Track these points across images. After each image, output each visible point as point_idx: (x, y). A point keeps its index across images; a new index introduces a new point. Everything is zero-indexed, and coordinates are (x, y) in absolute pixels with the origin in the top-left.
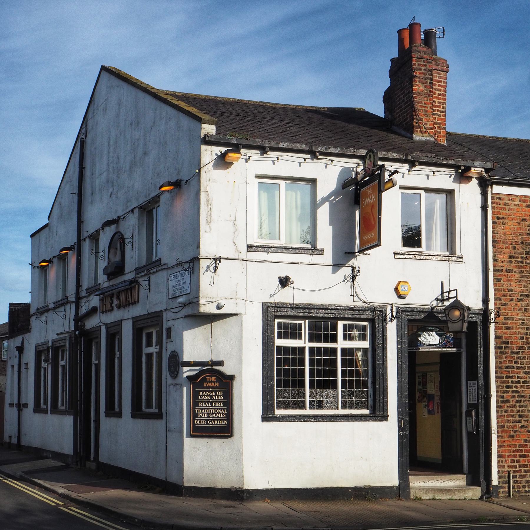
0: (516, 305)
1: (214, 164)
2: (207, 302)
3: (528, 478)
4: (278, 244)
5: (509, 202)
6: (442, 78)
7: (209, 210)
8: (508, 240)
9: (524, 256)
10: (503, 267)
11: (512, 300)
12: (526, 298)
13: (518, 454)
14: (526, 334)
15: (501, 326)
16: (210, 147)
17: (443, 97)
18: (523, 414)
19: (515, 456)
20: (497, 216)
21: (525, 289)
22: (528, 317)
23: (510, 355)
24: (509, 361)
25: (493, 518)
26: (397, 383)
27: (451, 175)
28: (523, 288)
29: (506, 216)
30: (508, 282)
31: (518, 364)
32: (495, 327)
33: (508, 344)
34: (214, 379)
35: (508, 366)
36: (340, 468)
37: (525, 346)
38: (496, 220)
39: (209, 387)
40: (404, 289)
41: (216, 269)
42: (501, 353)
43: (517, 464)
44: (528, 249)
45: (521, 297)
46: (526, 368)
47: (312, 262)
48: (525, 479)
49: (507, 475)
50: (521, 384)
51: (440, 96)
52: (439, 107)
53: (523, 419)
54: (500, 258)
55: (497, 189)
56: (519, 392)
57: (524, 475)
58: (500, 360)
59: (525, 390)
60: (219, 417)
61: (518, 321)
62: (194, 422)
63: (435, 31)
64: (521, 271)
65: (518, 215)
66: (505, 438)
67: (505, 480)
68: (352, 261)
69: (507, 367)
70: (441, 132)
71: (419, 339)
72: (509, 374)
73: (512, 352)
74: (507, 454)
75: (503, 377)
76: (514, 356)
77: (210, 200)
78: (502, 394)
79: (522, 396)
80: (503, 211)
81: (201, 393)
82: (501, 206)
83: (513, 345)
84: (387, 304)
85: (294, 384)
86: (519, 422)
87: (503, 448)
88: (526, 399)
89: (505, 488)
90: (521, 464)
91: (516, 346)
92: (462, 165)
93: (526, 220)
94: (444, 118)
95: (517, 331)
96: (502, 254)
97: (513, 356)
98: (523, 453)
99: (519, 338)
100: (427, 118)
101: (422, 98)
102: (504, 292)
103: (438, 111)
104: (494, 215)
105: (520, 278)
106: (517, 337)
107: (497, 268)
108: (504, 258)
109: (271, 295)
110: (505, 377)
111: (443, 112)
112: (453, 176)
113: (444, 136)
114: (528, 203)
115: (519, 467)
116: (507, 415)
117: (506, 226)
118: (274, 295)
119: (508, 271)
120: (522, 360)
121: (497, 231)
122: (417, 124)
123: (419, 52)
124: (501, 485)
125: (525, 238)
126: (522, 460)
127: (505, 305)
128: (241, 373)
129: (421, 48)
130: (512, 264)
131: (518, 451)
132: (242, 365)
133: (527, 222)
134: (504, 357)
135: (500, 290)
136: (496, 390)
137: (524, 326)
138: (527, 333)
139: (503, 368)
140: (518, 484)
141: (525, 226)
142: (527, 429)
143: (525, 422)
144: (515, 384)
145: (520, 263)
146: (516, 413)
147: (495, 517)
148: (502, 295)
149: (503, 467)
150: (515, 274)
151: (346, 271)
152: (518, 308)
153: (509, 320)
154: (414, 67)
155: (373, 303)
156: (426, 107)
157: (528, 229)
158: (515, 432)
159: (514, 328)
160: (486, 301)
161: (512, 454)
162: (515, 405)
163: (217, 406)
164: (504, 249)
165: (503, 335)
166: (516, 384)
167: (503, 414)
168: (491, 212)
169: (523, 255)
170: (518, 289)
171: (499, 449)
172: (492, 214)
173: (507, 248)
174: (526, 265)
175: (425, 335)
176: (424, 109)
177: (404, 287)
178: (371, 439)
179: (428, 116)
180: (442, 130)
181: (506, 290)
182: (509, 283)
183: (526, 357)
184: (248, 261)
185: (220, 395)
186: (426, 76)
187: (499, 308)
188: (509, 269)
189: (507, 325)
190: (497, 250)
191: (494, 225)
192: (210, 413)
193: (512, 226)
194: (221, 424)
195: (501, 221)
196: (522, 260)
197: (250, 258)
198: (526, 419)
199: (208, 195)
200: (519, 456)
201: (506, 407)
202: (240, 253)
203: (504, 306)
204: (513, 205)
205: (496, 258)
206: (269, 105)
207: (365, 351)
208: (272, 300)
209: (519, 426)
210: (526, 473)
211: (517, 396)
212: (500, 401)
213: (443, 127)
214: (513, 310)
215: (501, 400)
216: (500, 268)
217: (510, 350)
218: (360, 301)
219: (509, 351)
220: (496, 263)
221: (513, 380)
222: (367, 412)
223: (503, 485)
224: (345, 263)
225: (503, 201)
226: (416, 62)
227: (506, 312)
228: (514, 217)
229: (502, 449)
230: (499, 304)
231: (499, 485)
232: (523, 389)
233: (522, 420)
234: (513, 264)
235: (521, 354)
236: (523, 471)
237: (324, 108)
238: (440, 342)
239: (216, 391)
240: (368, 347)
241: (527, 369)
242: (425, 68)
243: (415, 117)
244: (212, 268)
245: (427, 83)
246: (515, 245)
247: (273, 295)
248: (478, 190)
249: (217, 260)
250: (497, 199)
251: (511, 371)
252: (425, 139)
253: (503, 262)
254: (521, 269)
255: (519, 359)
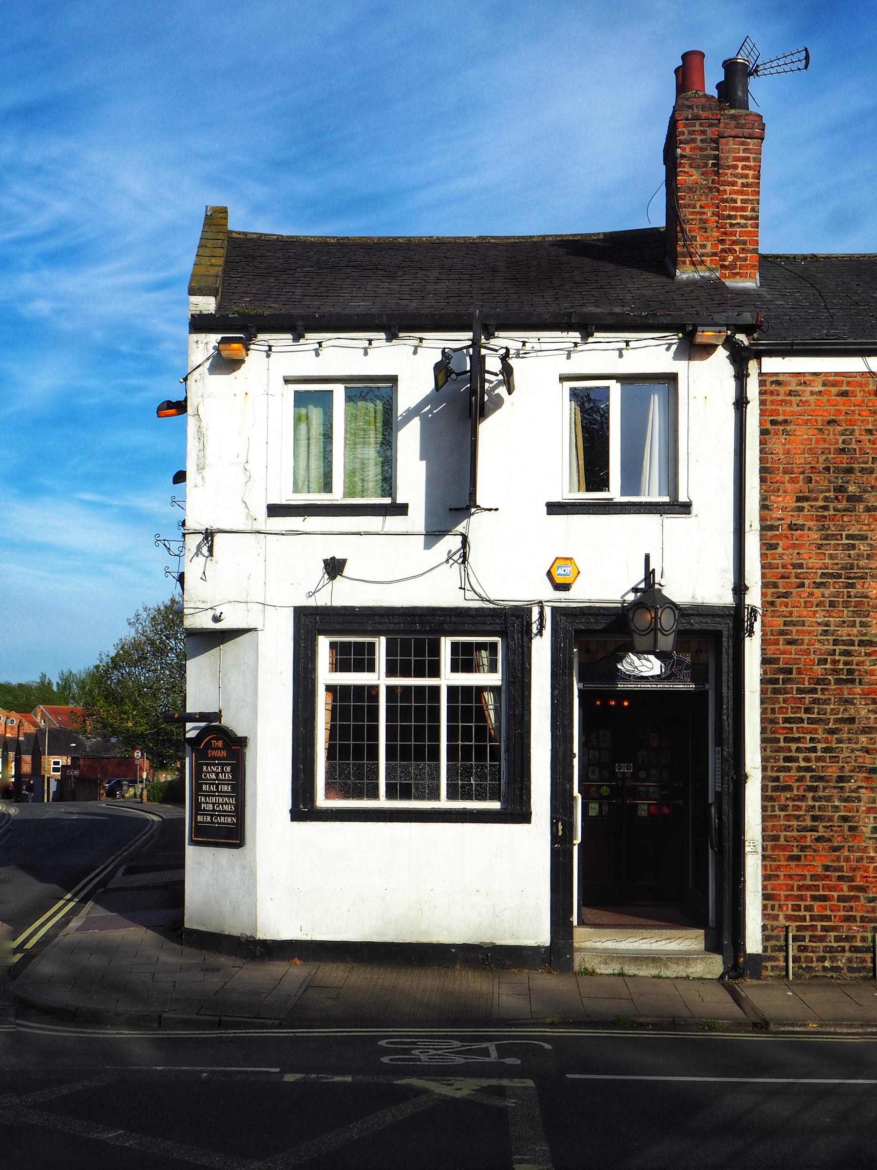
0: (811, 594)
1: (211, 365)
2: (197, 610)
3: (831, 942)
4: (329, 500)
5: (798, 388)
6: (751, 151)
7: (201, 447)
8: (794, 466)
9: (831, 494)
10: (783, 519)
11: (802, 585)
12: (835, 580)
13: (809, 893)
14: (832, 652)
15: (776, 637)
16: (204, 335)
17: (752, 189)
18: (821, 813)
19: (802, 898)
20: (772, 418)
21: (832, 561)
22: (837, 619)
23: (795, 696)
24: (792, 708)
25: (649, 1020)
26: (550, 752)
27: (670, 345)
28: (827, 561)
29: (791, 418)
30: (794, 549)
31: (813, 713)
32: (762, 640)
33: (791, 673)
34: (220, 743)
35: (790, 718)
36: (435, 907)
37: (830, 677)
38: (769, 426)
39: (214, 758)
40: (562, 572)
41: (211, 549)
42: (775, 691)
43: (805, 913)
44: (840, 481)
45: (821, 578)
46: (832, 721)
47: (386, 530)
48: (825, 944)
49: (783, 934)
50: (819, 754)
51: (745, 189)
52: (744, 209)
53: (821, 825)
54: (775, 502)
55: (772, 365)
56: (813, 770)
57: (820, 936)
58: (773, 706)
59: (828, 766)
60: (225, 811)
61: (815, 628)
62: (196, 818)
63: (742, 61)
64: (824, 525)
65: (819, 413)
66: (780, 861)
67: (778, 944)
68: (464, 523)
69: (786, 720)
70: (749, 258)
71: (619, 666)
72: (793, 733)
73: (798, 689)
74: (782, 893)
75: (778, 740)
76: (805, 698)
77: (204, 430)
78: (775, 774)
79: (821, 779)
80: (784, 408)
81: (205, 768)
82: (780, 398)
83: (803, 676)
84: (533, 603)
85: (358, 752)
86: (814, 829)
87: (775, 880)
88: (829, 784)
89: (779, 960)
90: (816, 913)
91: (809, 678)
92: (688, 324)
93: (836, 422)
94: (756, 229)
95: (812, 648)
96: (780, 493)
97: (802, 698)
98: (821, 893)
99: (817, 662)
100: (707, 234)
101: (695, 197)
102: (783, 570)
103: (742, 217)
104: (766, 418)
105: (821, 539)
106: (810, 660)
107: (769, 523)
108: (785, 501)
109: (311, 594)
110: (782, 740)
111: (752, 218)
112: (674, 347)
113: (755, 266)
114: (842, 386)
115: (811, 920)
116: (786, 815)
117: (792, 437)
118: (315, 592)
119: (794, 528)
120: (822, 706)
121: (771, 449)
122: (685, 249)
123: (691, 107)
124: (769, 953)
125: (835, 458)
126: (819, 906)
127: (786, 595)
128: (255, 734)
129: (695, 100)
130: (802, 513)
131: (808, 888)
132: (257, 719)
133: (839, 425)
134: (781, 699)
135: (776, 566)
136: (762, 766)
137: (829, 638)
138: (835, 650)
139: (779, 722)
140: (808, 954)
141: (835, 435)
142: (830, 844)
143: (826, 830)
144: (804, 754)
145: (821, 510)
146: (806, 811)
147: (655, 1020)
148: (780, 575)
149: (776, 917)
150: (809, 532)
151: (451, 542)
152: (815, 601)
153: (794, 625)
154: (681, 138)
155: (503, 601)
156: (704, 213)
157: (840, 441)
158: (803, 849)
159: (806, 642)
160: (740, 589)
161: (796, 893)
162: (804, 796)
163: (224, 792)
164: (787, 483)
165: (779, 656)
166: (808, 754)
167: (777, 813)
168: (759, 411)
169: (828, 494)
170: (814, 561)
171: (765, 883)
172: (760, 415)
173: (793, 481)
174: (835, 513)
175: (631, 659)
176: (699, 217)
177: (563, 568)
178: (496, 856)
179: (709, 231)
180: (749, 255)
181: (789, 567)
182: (796, 551)
183: (830, 699)
184: (268, 534)
185: (227, 772)
186: (705, 153)
187: (773, 601)
188: (795, 524)
189: (789, 637)
190: (770, 487)
191: (765, 437)
192: (216, 803)
193: (805, 436)
194: (228, 824)
195: (781, 428)
196: (825, 504)
197: (271, 529)
198: (828, 824)
199: (200, 420)
200: (810, 898)
201: (783, 799)
202: (254, 521)
203: (783, 597)
204: (807, 393)
205: (767, 503)
206: (492, 241)
207: (494, 689)
208: (311, 602)
209: (811, 838)
210: (827, 931)
211: (808, 778)
212: (770, 787)
213: (752, 247)
214: (803, 605)
215: (772, 786)
216: (776, 523)
217: (795, 686)
218: (478, 598)
219: (792, 688)
220: (767, 512)
221: (801, 745)
222: (496, 805)
223: (773, 954)
224: (448, 529)
225: (785, 388)
226: (684, 127)
227: (788, 609)
228: (810, 417)
229: (771, 882)
230: (773, 593)
231: (765, 954)
232: (824, 764)
233: (820, 827)
234: (806, 512)
235: (819, 692)
236: (819, 928)
237: (599, 234)
238: (663, 670)
239: (223, 765)
240: (499, 683)
241: (833, 724)
242: (704, 137)
243: (680, 235)
244: (205, 550)
245: (706, 165)
246: (811, 475)
247: (313, 594)
248: (729, 370)
249: (209, 535)
250: (771, 385)
251: (797, 727)
252: (701, 277)
253: (784, 509)
254: (823, 521)
255: (814, 703)
